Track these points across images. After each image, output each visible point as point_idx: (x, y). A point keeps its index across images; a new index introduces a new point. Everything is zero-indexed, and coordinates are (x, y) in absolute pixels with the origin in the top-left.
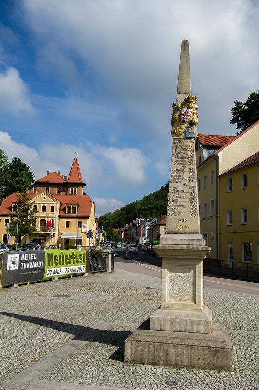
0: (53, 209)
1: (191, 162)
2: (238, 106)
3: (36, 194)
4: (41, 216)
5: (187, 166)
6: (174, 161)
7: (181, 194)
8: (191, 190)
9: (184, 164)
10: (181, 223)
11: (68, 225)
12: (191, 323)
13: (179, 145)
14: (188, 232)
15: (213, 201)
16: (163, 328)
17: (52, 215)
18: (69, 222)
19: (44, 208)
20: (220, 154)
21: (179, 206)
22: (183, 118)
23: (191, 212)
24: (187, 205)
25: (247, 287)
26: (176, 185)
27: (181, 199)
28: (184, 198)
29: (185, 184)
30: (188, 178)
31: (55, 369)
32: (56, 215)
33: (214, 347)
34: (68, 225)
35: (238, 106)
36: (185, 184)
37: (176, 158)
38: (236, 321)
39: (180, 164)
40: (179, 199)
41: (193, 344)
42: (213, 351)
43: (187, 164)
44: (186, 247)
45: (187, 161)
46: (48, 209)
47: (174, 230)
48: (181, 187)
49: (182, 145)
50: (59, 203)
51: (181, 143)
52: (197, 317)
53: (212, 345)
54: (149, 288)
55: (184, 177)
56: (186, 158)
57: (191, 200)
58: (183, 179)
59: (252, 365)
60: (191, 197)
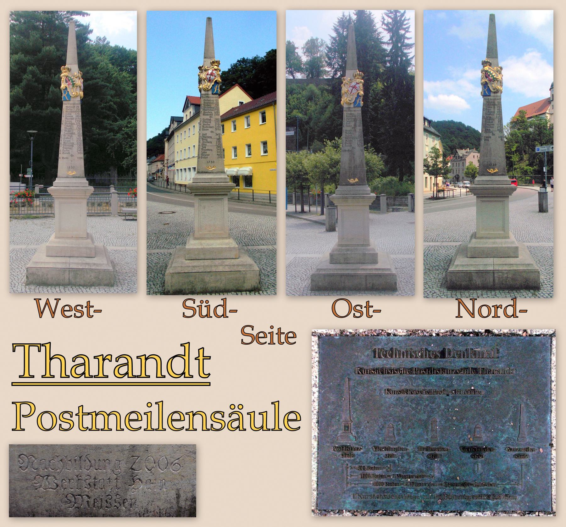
7: (209, 140)
8: (218, 137)
9: (211, 115)
14: (82, 282)
21: (208, 150)
29: (212, 132)
36: (212, 132)
40: (208, 144)
45: (213, 112)
49: (209, 99)
54: (161, 213)
58: (210, 127)
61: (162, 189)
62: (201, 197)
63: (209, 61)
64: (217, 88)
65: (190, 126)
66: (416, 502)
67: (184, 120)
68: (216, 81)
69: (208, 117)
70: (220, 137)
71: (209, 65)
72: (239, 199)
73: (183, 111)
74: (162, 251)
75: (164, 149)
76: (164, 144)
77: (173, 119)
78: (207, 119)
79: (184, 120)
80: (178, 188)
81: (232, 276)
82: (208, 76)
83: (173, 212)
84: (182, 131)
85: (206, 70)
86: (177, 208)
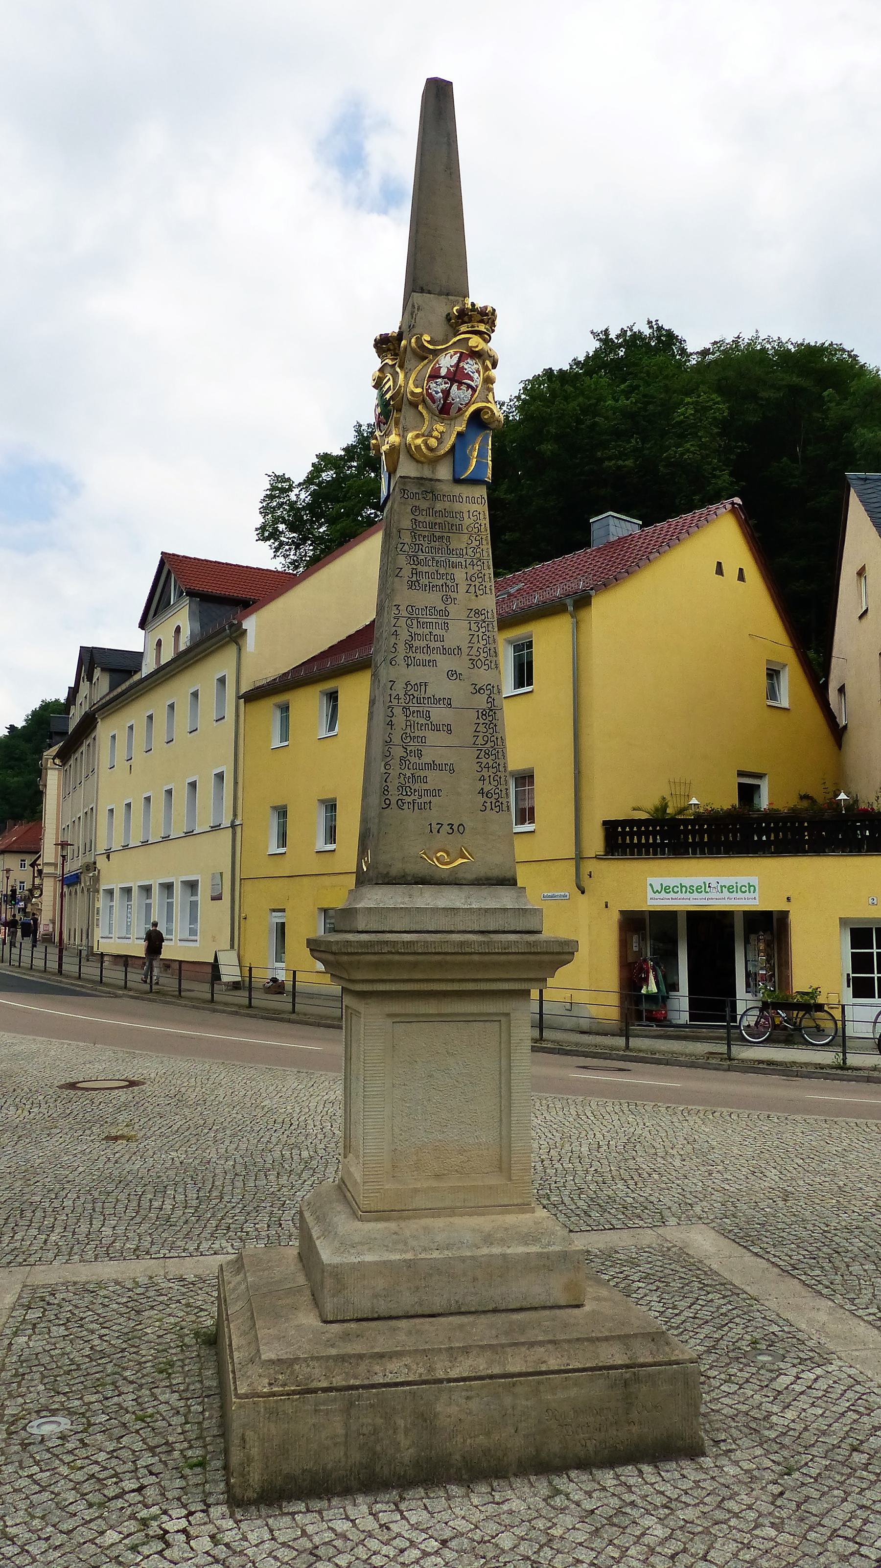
2: (280, 486)
6: (406, 572)
7: (438, 714)
8: (481, 701)
9: (448, 590)
12: (506, 1267)
13: (424, 505)
15: (220, 777)
16: (383, 1307)
21: (433, 766)
23: (481, 791)
25: (732, 1088)
28: (450, 731)
29: (452, 674)
30: (465, 650)
33: (627, 1366)
35: (280, 486)
36: (452, 674)
37: (414, 559)
40: (433, 738)
41: (544, 1368)
43: (462, 588)
44: (481, 943)
45: (460, 575)
47: (413, 868)
48: (440, 687)
49: (439, 506)
51: (435, 498)
52: (527, 1238)
53: (615, 1355)
54: (72, 1086)
56: (454, 566)
57: (480, 741)
58: (445, 651)
60: (481, 728)
61: (34, 977)
62: (396, 1007)
63: (437, 308)
64: (482, 454)
65: (178, 691)
67: (148, 667)
68: (477, 413)
70: (491, 700)
71: (440, 328)
73: (143, 625)
74: (108, 1270)
75: (37, 797)
76: (39, 772)
77: (91, 660)
78: (431, 610)
79: (148, 667)
80: (114, 974)
81: (573, 1392)
82: (437, 388)
83: (132, 1084)
84: (134, 715)
85: (423, 354)
86: (146, 1066)
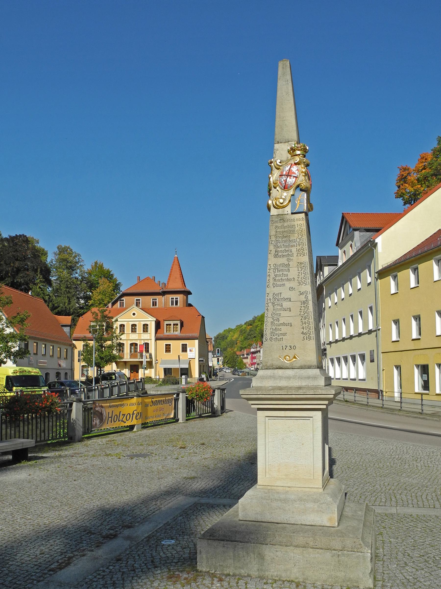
0: (145, 328)
1: (300, 253)
3: (122, 309)
4: (131, 338)
5: (295, 258)
7: (286, 304)
8: (303, 298)
9: (289, 256)
10: (287, 352)
11: (168, 349)
13: (279, 225)
14: (298, 365)
17: (145, 336)
18: (170, 345)
19: (134, 328)
20: (379, 240)
21: (284, 324)
22: (286, 181)
24: (297, 322)
26: (277, 290)
27: (287, 313)
29: (291, 289)
30: (296, 279)
31: (86, 583)
32: (151, 336)
34: (168, 349)
36: (291, 289)
38: (391, 491)
39: (283, 256)
40: (283, 313)
42: (338, 555)
43: (295, 255)
45: (294, 250)
46: (140, 328)
48: (286, 294)
50: (155, 319)
55: (290, 277)
56: (292, 246)
57: (302, 313)
58: (289, 280)
59: (405, 574)
60: (303, 308)
66: (248, 330)
69: (283, 260)
72: (430, 507)
78: (283, 265)
